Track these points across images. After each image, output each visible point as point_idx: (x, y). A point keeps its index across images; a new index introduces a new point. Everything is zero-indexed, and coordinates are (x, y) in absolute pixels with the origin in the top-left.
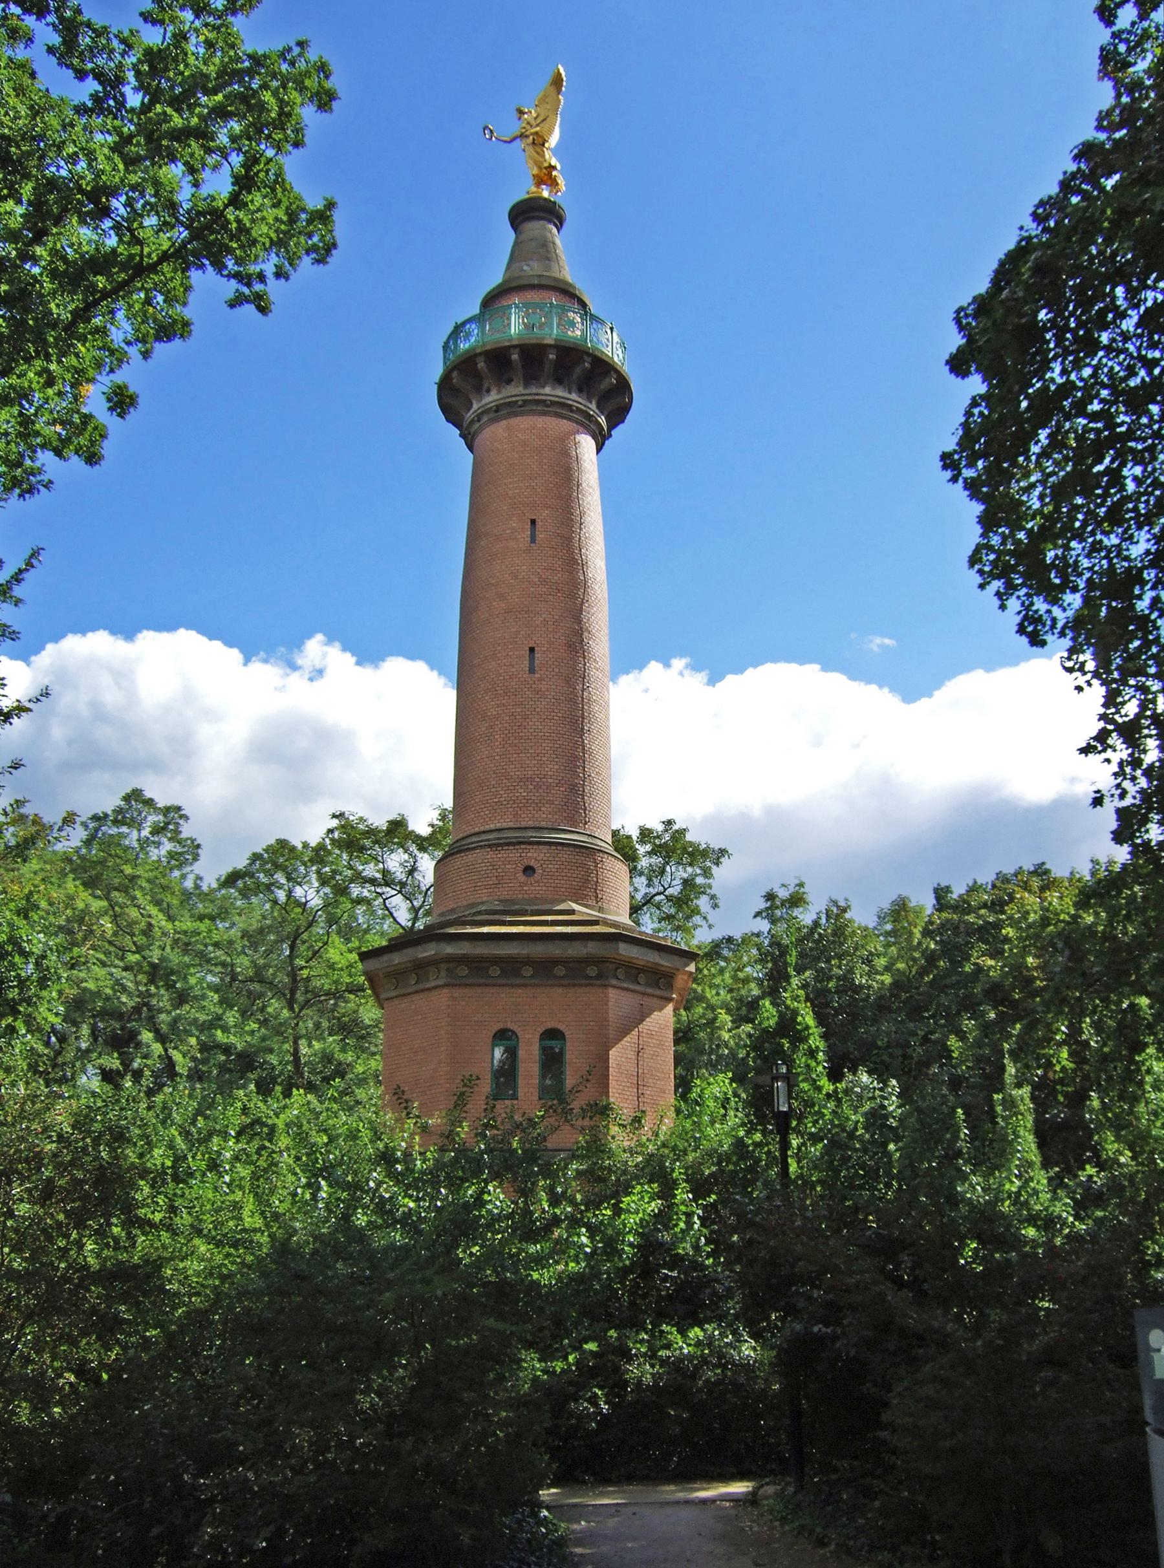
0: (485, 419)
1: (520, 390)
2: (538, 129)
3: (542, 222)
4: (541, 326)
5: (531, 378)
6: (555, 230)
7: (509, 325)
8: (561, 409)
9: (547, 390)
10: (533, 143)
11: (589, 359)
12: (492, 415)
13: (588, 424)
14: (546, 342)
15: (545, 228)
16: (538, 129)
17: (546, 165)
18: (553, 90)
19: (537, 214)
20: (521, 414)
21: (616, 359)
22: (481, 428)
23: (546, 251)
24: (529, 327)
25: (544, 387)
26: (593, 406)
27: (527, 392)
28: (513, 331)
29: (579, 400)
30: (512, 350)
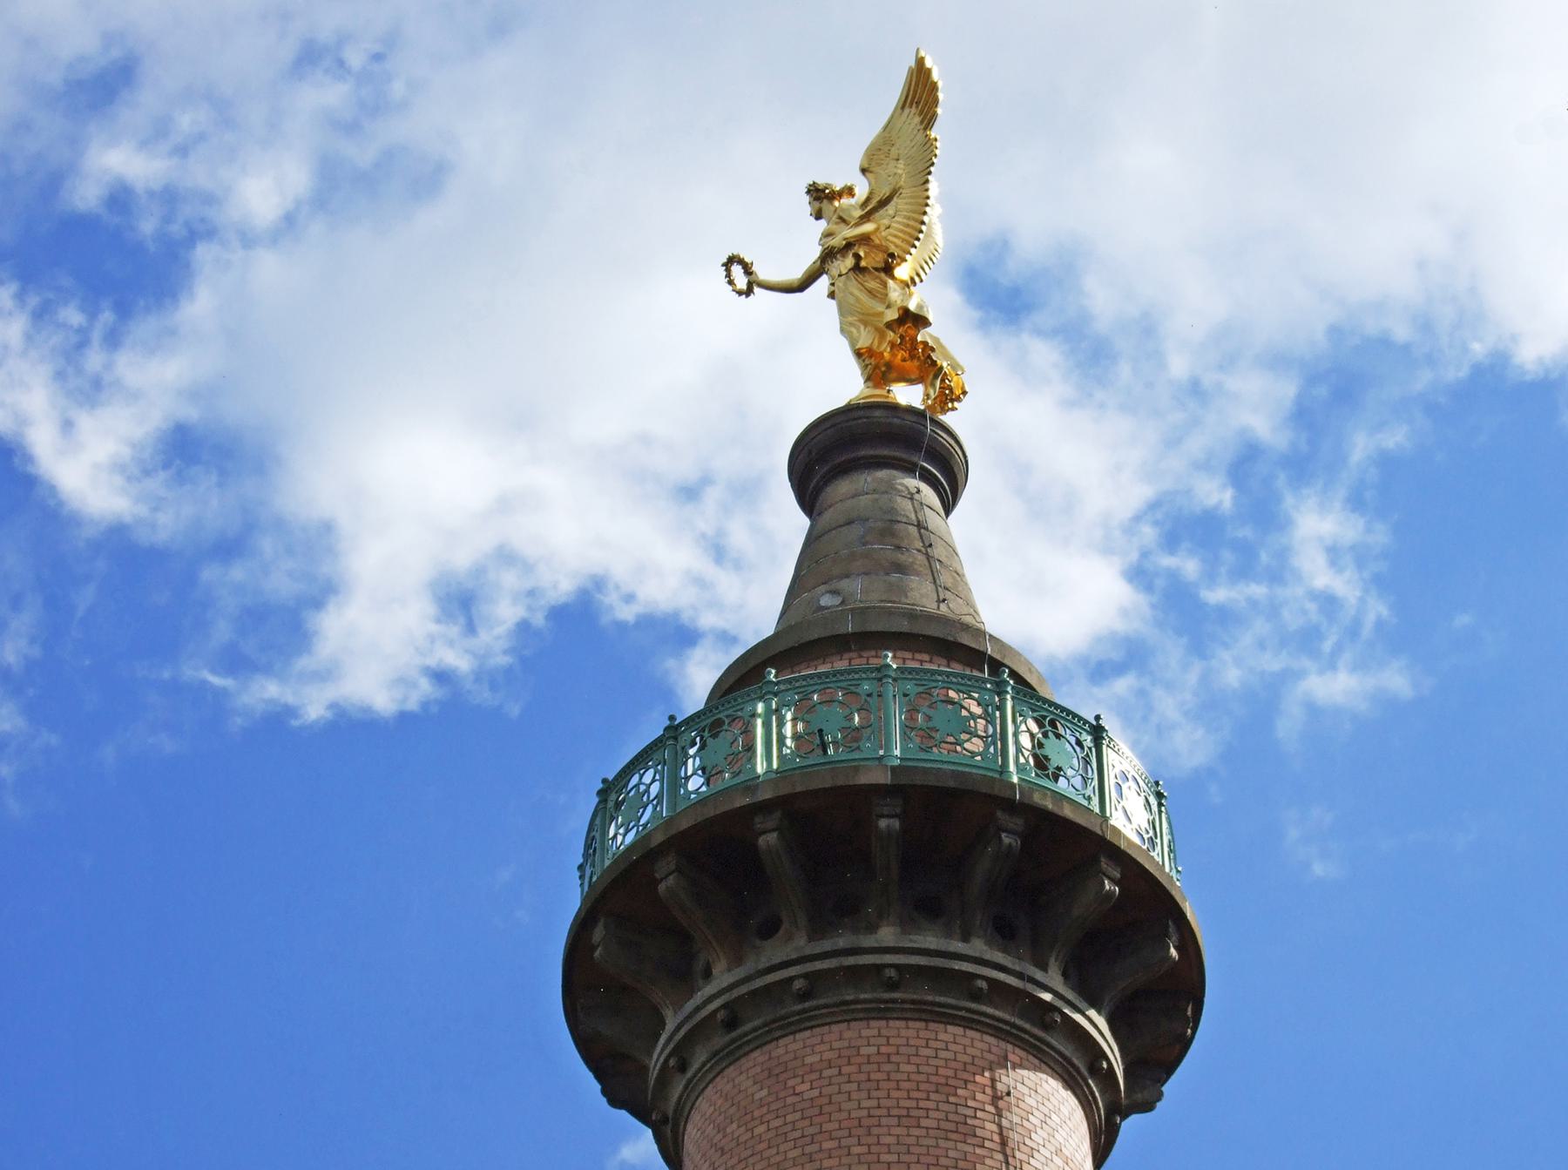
0: (699, 1057)
1: (800, 944)
2: (868, 227)
3: (882, 474)
4: (853, 736)
5: (836, 907)
6: (929, 495)
7: (750, 748)
8: (939, 994)
9: (887, 935)
10: (857, 268)
11: (1017, 823)
12: (719, 1041)
13: (1078, 1067)
14: (864, 779)
15: (890, 488)
16: (868, 227)
17: (892, 315)
18: (913, 118)
19: (865, 452)
20: (803, 1022)
21: (1117, 820)
22: (693, 1091)
23: (900, 548)
24: (813, 740)
25: (872, 928)
26: (1054, 978)
27: (826, 945)
28: (760, 768)
29: (999, 957)
30: (759, 822)
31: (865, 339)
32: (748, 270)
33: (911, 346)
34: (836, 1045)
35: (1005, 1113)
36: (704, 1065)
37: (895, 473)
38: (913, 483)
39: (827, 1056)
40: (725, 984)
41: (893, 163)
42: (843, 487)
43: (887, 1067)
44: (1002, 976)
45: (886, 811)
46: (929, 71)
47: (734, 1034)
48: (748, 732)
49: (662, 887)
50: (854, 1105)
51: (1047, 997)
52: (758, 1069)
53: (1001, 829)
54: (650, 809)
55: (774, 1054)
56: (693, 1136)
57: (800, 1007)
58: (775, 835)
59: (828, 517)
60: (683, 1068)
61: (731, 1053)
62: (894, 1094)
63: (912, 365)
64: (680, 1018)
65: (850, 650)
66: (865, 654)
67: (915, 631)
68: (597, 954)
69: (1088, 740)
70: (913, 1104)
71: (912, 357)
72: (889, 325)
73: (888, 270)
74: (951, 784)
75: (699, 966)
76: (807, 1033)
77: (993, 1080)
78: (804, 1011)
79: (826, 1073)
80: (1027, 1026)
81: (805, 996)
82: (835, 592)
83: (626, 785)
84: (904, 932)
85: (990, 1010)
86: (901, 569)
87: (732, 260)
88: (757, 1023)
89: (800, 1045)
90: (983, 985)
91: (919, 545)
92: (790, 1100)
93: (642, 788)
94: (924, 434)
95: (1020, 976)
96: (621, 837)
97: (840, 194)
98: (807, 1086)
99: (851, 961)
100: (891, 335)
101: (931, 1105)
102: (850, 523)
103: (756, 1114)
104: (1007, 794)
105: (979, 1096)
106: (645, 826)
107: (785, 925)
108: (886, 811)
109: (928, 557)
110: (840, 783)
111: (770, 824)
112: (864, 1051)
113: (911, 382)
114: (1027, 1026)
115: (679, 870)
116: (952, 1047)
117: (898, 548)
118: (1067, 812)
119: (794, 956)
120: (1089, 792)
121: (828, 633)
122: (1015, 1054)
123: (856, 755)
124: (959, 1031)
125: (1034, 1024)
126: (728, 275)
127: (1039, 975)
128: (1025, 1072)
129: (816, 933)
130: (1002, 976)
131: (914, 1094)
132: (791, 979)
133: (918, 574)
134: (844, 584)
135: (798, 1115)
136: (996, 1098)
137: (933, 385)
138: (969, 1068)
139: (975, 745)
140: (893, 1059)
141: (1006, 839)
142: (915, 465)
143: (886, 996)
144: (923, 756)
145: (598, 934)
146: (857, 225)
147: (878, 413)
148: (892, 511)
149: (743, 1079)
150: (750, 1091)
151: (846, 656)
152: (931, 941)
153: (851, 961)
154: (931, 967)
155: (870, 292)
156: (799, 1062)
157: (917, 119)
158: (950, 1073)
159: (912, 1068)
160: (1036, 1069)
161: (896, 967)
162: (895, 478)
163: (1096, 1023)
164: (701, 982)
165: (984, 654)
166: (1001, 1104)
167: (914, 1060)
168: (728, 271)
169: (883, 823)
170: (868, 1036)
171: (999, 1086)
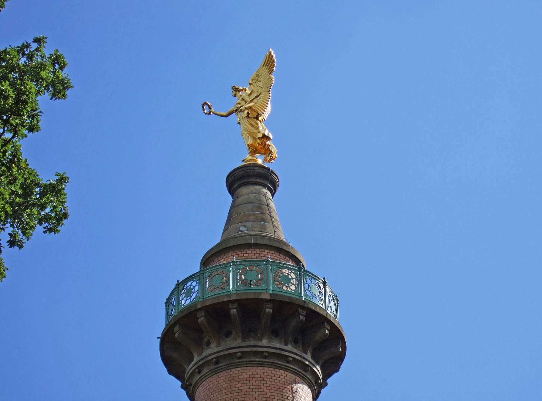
0: (205, 370)
1: (239, 342)
2: (252, 104)
3: (257, 187)
5: (249, 332)
7: (228, 281)
8: (278, 360)
9: (265, 342)
10: (248, 117)
12: (213, 367)
14: (263, 297)
15: (260, 193)
17: (260, 135)
18: (265, 70)
21: (329, 311)
22: (202, 379)
24: (247, 283)
25: (261, 340)
26: (309, 356)
29: (295, 351)
30: (231, 306)
31: (250, 141)
32: (209, 107)
33: (264, 145)
34: (248, 373)
35: (295, 398)
36: (207, 373)
37: (260, 187)
38: (266, 191)
39: (246, 376)
40: (216, 351)
41: (259, 83)
42: (244, 190)
43: (263, 382)
44: (296, 357)
45: (268, 306)
46: (272, 56)
47: (217, 366)
48: (228, 276)
49: (199, 320)
50: (254, 393)
51: (307, 363)
52: (224, 377)
53: (299, 314)
54: (195, 294)
55: (229, 373)
56: (200, 393)
57: (238, 361)
58: (236, 310)
59: (239, 200)
60: (199, 372)
61: (216, 371)
62: (265, 390)
63: (263, 151)
64: (200, 358)
65: (251, 248)
66: (256, 250)
67: (271, 244)
68: (176, 335)
69: (322, 286)
70: (270, 394)
71: (264, 147)
72: (259, 138)
73: (257, 118)
74: (287, 300)
75: (205, 341)
76: (240, 369)
77: (292, 387)
78: (239, 362)
79: (246, 382)
80: (301, 371)
81: (240, 358)
82: (245, 226)
83: (186, 284)
84: (269, 342)
85: (292, 366)
86: (264, 220)
87: (205, 104)
88: (225, 364)
89: (237, 372)
90: (291, 359)
91: (268, 212)
92: (235, 389)
93: (192, 287)
94: (269, 176)
95: (301, 356)
96: (185, 302)
97: (242, 90)
98: (240, 385)
99: (254, 349)
100: (258, 141)
101: (276, 395)
102: (248, 203)
103: (224, 391)
104: (302, 304)
105: (288, 392)
106: (193, 299)
107: (234, 333)
108: (268, 306)
109: (271, 216)
110: (256, 297)
111: (234, 307)
112: (257, 376)
113: (262, 154)
114: (301, 371)
115: (205, 316)
116: (281, 377)
117: (263, 213)
118: (318, 310)
119: (237, 346)
120: (322, 302)
121: (245, 242)
122: (298, 379)
123: (259, 288)
124: (283, 372)
125: (302, 370)
126: (203, 108)
127: (305, 356)
128: (300, 385)
129: (244, 339)
130: (296, 357)
131: (271, 391)
132: (237, 353)
133: (269, 223)
134: (247, 224)
135: (237, 394)
136: (293, 393)
137: (268, 156)
138: (286, 383)
139: (293, 288)
140: (265, 379)
141: (301, 317)
142: (266, 185)
143: (264, 360)
144: (279, 290)
145: (176, 329)
146: (249, 103)
147: (256, 168)
148: (261, 200)
149: (220, 379)
150: (222, 384)
151: (250, 250)
152: (277, 345)
153: (254, 349)
154: (277, 353)
155: (252, 125)
156: (237, 377)
157: (267, 71)
158: (281, 385)
159: (270, 383)
160: (302, 383)
161: (267, 352)
162: (261, 189)
163: (318, 370)
164: (206, 347)
165: (290, 253)
166: (294, 395)
167: (271, 380)
168: (203, 107)
169: (267, 310)
170: (258, 371)
171: (293, 389)
